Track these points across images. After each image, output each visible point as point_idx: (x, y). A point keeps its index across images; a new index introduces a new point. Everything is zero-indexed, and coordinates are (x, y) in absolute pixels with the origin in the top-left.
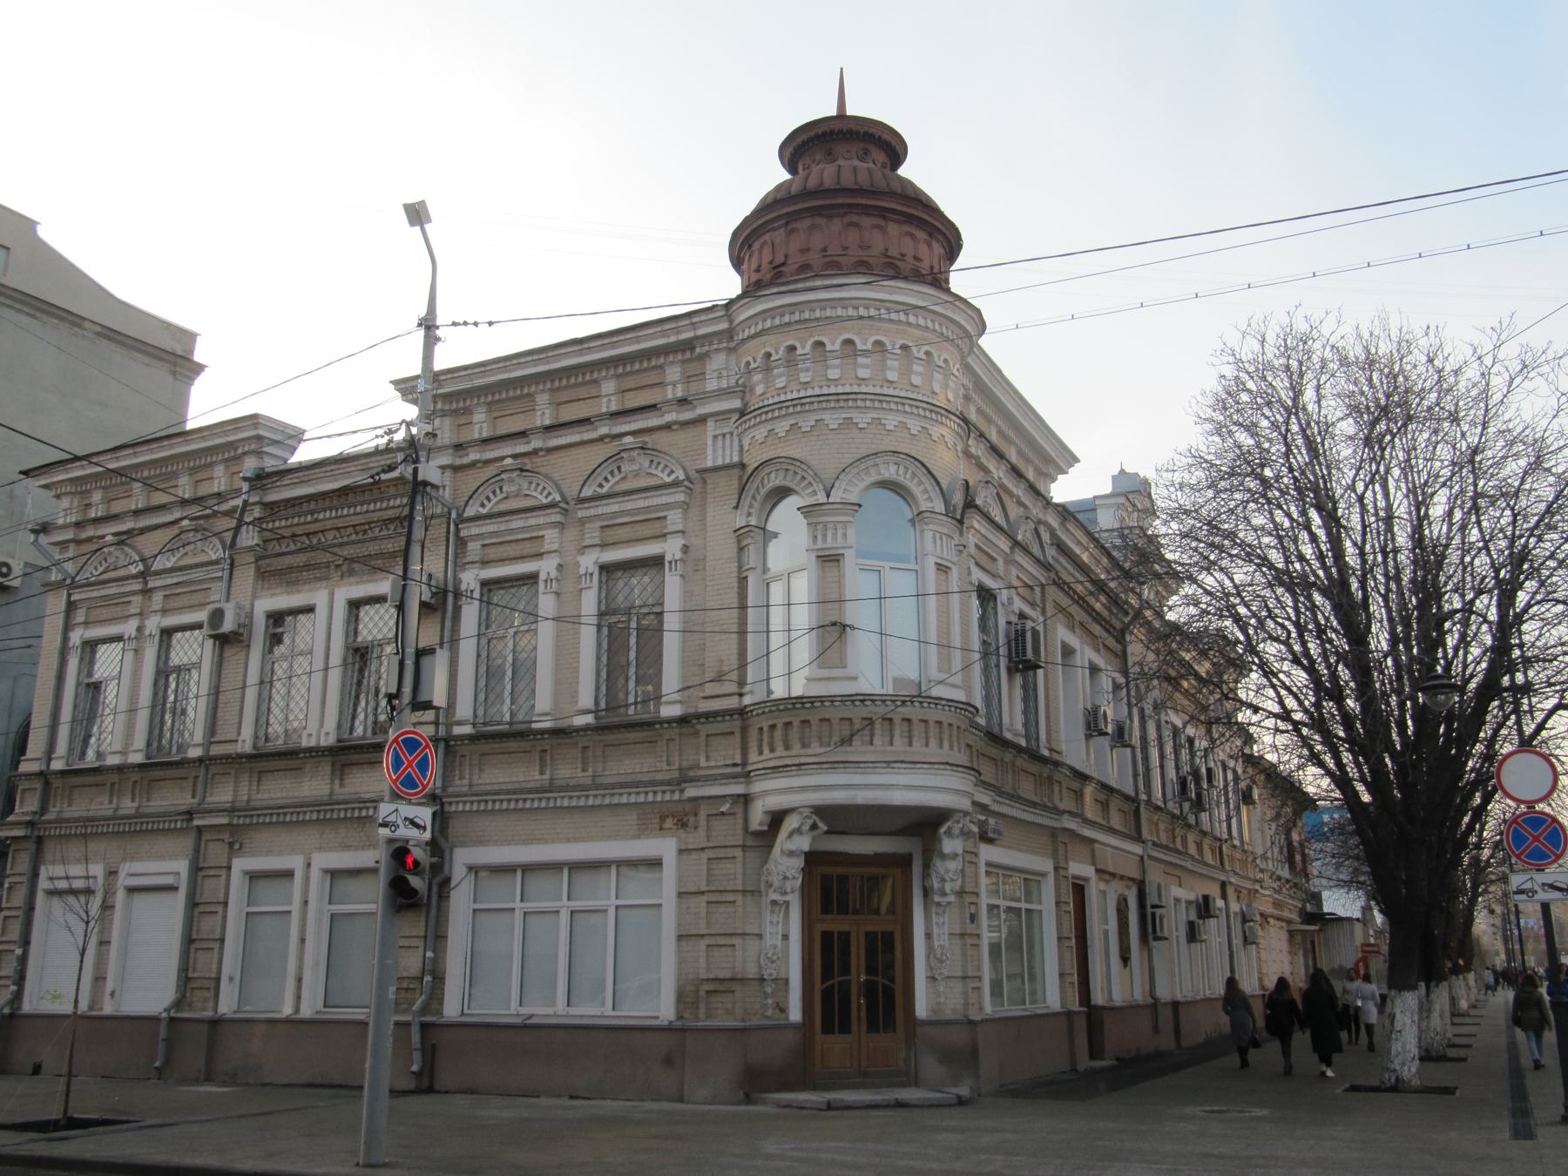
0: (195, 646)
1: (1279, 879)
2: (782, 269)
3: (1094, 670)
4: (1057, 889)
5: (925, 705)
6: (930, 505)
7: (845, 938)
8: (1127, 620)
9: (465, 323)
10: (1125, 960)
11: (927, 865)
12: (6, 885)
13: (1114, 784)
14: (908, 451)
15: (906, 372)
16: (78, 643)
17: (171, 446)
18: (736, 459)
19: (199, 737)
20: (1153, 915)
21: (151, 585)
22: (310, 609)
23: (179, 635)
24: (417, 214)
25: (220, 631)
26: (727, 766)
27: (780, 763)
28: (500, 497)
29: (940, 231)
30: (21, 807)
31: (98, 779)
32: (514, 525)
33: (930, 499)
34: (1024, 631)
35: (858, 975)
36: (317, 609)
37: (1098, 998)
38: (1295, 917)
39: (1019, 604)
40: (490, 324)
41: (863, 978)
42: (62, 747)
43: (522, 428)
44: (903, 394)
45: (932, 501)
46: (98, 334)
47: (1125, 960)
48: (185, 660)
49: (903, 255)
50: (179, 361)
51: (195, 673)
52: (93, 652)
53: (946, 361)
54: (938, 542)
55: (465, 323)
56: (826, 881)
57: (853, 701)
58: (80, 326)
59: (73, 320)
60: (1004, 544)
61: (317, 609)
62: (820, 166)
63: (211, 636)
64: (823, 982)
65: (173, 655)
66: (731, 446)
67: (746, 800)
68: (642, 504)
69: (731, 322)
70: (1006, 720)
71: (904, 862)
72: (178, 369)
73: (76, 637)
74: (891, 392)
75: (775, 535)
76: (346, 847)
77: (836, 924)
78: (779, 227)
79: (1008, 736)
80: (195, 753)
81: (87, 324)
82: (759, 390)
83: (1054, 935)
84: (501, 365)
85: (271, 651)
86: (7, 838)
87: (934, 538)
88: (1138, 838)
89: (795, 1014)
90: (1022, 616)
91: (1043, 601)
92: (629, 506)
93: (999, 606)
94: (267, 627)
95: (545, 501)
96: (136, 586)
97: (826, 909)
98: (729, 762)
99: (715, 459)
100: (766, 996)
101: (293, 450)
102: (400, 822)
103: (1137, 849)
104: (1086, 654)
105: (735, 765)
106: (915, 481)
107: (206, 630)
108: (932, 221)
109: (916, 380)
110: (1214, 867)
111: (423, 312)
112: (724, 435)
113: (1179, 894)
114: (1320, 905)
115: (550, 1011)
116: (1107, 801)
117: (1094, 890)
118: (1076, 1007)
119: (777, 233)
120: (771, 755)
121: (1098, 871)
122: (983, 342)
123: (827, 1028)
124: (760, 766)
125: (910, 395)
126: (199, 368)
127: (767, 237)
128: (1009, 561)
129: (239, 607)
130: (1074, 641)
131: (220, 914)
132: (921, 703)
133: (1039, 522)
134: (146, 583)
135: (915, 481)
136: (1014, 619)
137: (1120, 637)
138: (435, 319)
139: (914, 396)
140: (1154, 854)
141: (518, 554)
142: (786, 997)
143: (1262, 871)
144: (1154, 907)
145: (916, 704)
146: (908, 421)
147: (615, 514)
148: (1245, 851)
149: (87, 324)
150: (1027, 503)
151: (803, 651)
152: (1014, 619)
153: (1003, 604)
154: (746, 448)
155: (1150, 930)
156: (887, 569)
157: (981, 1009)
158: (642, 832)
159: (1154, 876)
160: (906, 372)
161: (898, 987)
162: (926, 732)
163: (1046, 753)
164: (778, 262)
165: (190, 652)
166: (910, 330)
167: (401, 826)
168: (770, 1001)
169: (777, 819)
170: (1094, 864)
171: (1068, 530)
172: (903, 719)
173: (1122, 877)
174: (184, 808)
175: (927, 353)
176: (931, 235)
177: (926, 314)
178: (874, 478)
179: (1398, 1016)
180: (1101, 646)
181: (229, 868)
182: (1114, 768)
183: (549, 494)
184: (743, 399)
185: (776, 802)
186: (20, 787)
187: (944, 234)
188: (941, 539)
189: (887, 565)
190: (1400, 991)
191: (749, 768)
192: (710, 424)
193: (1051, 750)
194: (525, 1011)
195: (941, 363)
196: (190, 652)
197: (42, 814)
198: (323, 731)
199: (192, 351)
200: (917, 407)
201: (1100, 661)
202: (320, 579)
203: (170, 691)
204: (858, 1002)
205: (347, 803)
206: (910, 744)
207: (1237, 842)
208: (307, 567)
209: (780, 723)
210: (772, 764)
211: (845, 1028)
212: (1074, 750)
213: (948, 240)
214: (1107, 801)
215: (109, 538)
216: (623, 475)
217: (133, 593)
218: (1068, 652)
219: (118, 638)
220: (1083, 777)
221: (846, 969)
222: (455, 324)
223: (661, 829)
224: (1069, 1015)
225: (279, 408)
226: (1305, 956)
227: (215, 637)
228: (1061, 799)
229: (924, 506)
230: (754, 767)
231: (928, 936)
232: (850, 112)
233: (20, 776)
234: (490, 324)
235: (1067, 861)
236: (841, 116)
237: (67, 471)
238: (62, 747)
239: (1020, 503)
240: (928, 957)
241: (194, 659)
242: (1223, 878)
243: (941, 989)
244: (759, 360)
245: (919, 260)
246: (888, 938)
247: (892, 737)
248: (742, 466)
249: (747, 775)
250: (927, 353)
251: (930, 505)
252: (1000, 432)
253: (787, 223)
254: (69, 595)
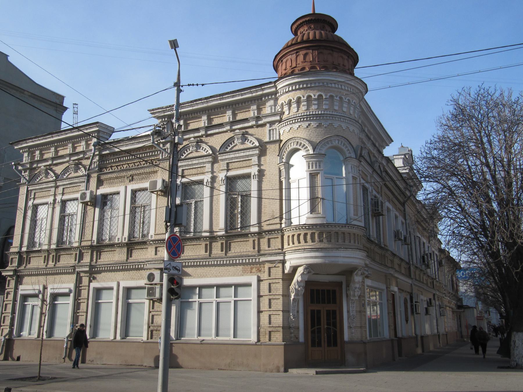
0: (75, 206)
1: (450, 293)
2: (295, 69)
3: (396, 217)
4: (387, 295)
5: (350, 227)
6: (350, 155)
7: (319, 312)
8: (405, 200)
9: (193, 85)
10: (407, 321)
11: (348, 286)
12: (6, 292)
13: (402, 258)
14: (342, 135)
15: (341, 106)
16: (31, 205)
17: (66, 134)
18: (278, 138)
19: (77, 239)
20: (416, 305)
21: (58, 184)
22: (118, 193)
23: (69, 202)
24: (174, 44)
25: (85, 201)
26: (276, 249)
27: (296, 248)
28: (189, 152)
29: (352, 56)
30: (11, 264)
31: (40, 254)
32: (194, 162)
33: (350, 153)
34: (378, 202)
35: (324, 325)
36: (121, 193)
37: (399, 335)
38: (454, 307)
39: (374, 193)
40: (203, 85)
41: (326, 326)
42: (25, 243)
43: (197, 127)
44: (340, 114)
45: (350, 154)
46: (30, 96)
47: (407, 321)
48: (71, 211)
49: (339, 64)
50: (58, 106)
51: (75, 217)
52: (37, 208)
53: (354, 103)
54: (353, 169)
55: (193, 85)
56: (312, 291)
57: (324, 226)
58: (23, 93)
59: (21, 90)
60: (370, 171)
61: (121, 193)
62: (308, 31)
63: (81, 203)
64: (311, 328)
65: (67, 209)
66: (276, 133)
67: (283, 262)
68: (242, 154)
69: (276, 88)
70: (371, 234)
71: (340, 284)
72: (58, 109)
73: (30, 203)
74: (336, 114)
75: (292, 166)
76: (133, 279)
77: (316, 307)
78: (293, 54)
79: (372, 239)
80: (76, 245)
81: (26, 93)
82: (287, 113)
83: (387, 312)
84: (161, 110)
85: (103, 208)
86: (6, 275)
87: (352, 167)
88: (409, 276)
89: (302, 339)
90: (375, 197)
91: (381, 192)
92: (237, 155)
93: (369, 193)
94: (102, 199)
95: (206, 154)
96: (53, 184)
97: (312, 302)
98: (277, 248)
99: (270, 138)
100: (291, 333)
101: (110, 136)
102: (171, 268)
103: (410, 281)
104: (394, 212)
105: (279, 249)
106: (345, 147)
107: (80, 201)
108: (349, 52)
109: (345, 110)
110: (430, 288)
111: (176, 81)
112: (273, 130)
113: (423, 298)
114: (462, 302)
115: (227, 338)
116: (400, 264)
117: (397, 295)
118: (394, 338)
119: (293, 56)
120: (293, 246)
121: (399, 289)
122: (366, 97)
123: (313, 344)
124: (289, 249)
125: (342, 115)
126: (66, 109)
127: (289, 57)
128: (372, 177)
129: (92, 192)
130: (391, 207)
131: (86, 303)
132: (348, 227)
133: (380, 163)
134: (56, 184)
135: (345, 147)
136: (373, 197)
137: (403, 205)
138: (180, 83)
139: (344, 115)
140: (416, 283)
141: (196, 173)
142: (298, 333)
143: (445, 290)
144: (416, 302)
145: (347, 227)
146: (342, 124)
147: (232, 158)
148: (440, 283)
149: (26, 93)
150: (376, 156)
151: (306, 207)
152: (373, 197)
153: (370, 192)
154: (281, 134)
155: (414, 310)
156: (335, 178)
157: (366, 338)
158: (244, 273)
159: (415, 291)
160: (341, 106)
161: (338, 330)
162: (350, 237)
163: (383, 246)
164: (293, 67)
165: (73, 209)
166: (342, 91)
167: (172, 269)
168: (293, 335)
169: (294, 269)
170: (397, 286)
171: (389, 166)
172: (342, 233)
173: (406, 291)
174: (72, 265)
175: (348, 100)
176: (348, 57)
177: (348, 86)
178: (330, 145)
179: (517, 341)
180: (398, 209)
181: (89, 286)
182: (402, 252)
183: (254, 143)
184: (280, 117)
185: (295, 263)
186: (11, 257)
187: (353, 57)
188: (354, 167)
189: (335, 176)
190: (517, 332)
191: (284, 250)
192: (268, 125)
193: (385, 245)
194: (201, 338)
195: (353, 103)
196: (73, 209)
197: (18, 268)
198: (124, 237)
199: (63, 103)
200: (345, 119)
201: (398, 214)
202: (122, 182)
203: (66, 222)
204: (324, 336)
205: (133, 263)
206: (344, 242)
207: (437, 280)
208: (117, 178)
209: (296, 234)
210: (294, 249)
211: (319, 345)
212: (393, 246)
213: (354, 58)
214: (400, 264)
215: (192, 139)
216: (235, 144)
217: (52, 187)
218: (388, 210)
219: (46, 203)
220: (394, 255)
221: (319, 323)
222: (189, 85)
223: (251, 272)
224: (392, 340)
225: (107, 120)
226: (457, 320)
227: (82, 203)
228: (388, 263)
229: (348, 155)
230: (287, 250)
231: (348, 312)
232: (316, 12)
233: (11, 253)
234: (203, 85)
235: (390, 286)
236: (314, 14)
237: (27, 143)
238: (25, 243)
239: (374, 156)
240: (348, 319)
241: (75, 211)
242: (434, 292)
243: (353, 331)
244: (295, 99)
245: (345, 66)
246: (334, 312)
247: (338, 239)
248: (281, 141)
249: (284, 254)
250: (348, 100)
251: (350, 155)
252: (368, 130)
253: (297, 53)
254: (28, 188)
